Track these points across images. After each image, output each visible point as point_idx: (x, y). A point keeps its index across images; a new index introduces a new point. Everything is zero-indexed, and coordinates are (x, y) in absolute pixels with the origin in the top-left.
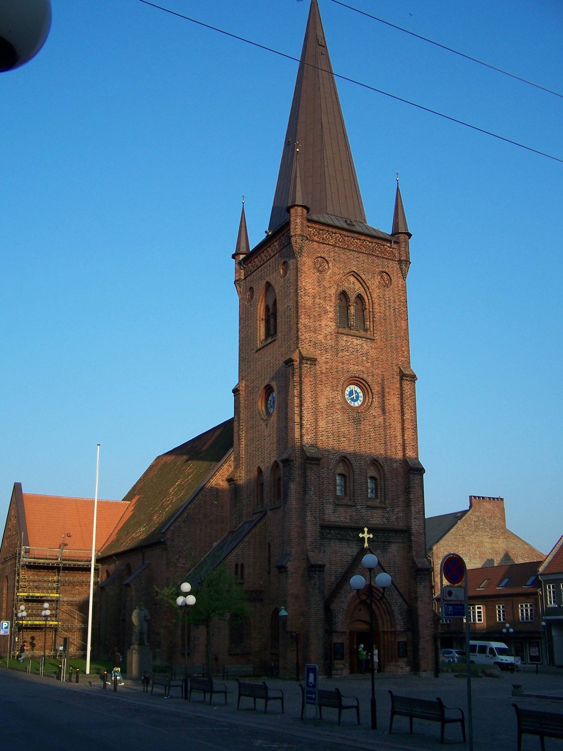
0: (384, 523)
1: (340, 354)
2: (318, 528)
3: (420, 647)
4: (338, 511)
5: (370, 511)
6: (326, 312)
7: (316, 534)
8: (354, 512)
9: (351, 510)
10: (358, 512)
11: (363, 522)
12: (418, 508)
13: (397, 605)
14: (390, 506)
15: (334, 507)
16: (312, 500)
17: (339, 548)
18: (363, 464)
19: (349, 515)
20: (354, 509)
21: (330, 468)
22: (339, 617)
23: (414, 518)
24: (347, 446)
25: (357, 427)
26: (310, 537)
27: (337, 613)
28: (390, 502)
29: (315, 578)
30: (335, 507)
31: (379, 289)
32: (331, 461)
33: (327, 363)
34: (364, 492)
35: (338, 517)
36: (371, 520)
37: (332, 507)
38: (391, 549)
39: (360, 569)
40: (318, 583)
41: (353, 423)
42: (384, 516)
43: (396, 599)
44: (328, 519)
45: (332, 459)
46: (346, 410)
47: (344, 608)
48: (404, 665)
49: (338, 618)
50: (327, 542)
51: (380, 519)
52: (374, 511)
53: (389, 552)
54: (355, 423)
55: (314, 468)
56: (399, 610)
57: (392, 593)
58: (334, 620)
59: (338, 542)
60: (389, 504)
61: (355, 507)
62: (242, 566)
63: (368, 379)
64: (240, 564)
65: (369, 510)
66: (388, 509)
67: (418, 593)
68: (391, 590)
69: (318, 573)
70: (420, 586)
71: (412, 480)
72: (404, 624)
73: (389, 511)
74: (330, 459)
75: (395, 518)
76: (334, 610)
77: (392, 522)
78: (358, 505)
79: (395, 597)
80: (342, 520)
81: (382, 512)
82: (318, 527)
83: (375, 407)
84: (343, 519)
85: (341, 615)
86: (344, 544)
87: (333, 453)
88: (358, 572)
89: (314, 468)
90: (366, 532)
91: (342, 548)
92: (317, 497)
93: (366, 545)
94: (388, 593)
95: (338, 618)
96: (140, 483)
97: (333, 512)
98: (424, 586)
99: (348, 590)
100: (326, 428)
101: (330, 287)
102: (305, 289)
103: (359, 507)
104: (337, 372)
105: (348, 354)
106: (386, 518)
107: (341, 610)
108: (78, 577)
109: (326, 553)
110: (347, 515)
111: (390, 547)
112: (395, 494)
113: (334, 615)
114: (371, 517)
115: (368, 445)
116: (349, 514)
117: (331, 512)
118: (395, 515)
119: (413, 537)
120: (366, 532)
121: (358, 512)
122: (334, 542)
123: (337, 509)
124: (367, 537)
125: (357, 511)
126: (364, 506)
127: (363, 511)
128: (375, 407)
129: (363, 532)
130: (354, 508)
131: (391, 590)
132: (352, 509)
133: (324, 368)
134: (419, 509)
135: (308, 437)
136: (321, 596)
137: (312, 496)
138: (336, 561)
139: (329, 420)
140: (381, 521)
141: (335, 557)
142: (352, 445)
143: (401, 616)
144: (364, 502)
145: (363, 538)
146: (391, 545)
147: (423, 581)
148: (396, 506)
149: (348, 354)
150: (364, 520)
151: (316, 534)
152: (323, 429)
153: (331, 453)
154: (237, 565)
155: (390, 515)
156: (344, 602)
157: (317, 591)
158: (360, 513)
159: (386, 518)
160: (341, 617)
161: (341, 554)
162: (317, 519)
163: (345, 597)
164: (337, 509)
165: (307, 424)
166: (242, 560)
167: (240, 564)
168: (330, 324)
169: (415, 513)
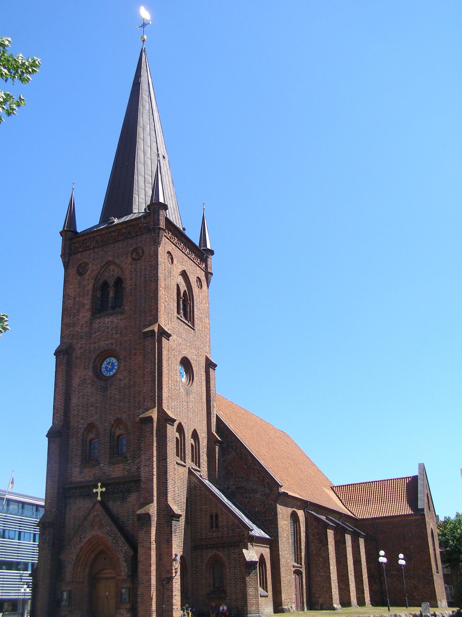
0: (125, 475)
1: (93, 336)
2: (56, 491)
3: (139, 593)
4: (84, 472)
5: (111, 467)
6: (84, 305)
7: (54, 496)
8: (98, 470)
9: (94, 469)
10: (101, 470)
11: (105, 477)
12: (148, 455)
13: (121, 552)
14: (131, 458)
15: (80, 469)
16: (53, 467)
17: (83, 504)
18: (108, 425)
19: (93, 474)
20: (97, 467)
21: (79, 436)
22: (68, 567)
23: (144, 466)
24: (94, 413)
25: (104, 394)
26: (49, 499)
27: (66, 563)
28: (131, 455)
29: (46, 534)
30: (81, 469)
31: (131, 265)
32: (80, 429)
33: (81, 348)
34: (107, 450)
35: (83, 478)
36: (112, 475)
37: (78, 470)
38: (131, 498)
39: (89, 521)
40: (48, 538)
41: (100, 391)
42: (125, 468)
43: (122, 546)
44: (75, 481)
45: (81, 428)
46: (95, 382)
47: (73, 559)
48: (126, 612)
49: (67, 567)
50: (73, 500)
51: (121, 472)
52: (115, 466)
53: (129, 502)
54: (102, 391)
55: (56, 440)
56: (124, 557)
57: (117, 541)
58: (64, 570)
59: (82, 499)
60: (130, 456)
61: (98, 466)
62: (217, 515)
63: (116, 348)
64: (214, 514)
65: (111, 466)
66: (129, 462)
67: (139, 539)
68: (117, 538)
69: (49, 530)
70: (141, 532)
71: (144, 429)
72: (128, 571)
73: (130, 463)
74: (79, 428)
75: (136, 469)
76: (65, 561)
77: (132, 473)
78: (102, 463)
79: (120, 545)
80: (87, 480)
81: (123, 466)
82: (56, 490)
83: (122, 371)
84: (87, 478)
85: (70, 565)
86: (87, 501)
87: (82, 423)
88: (87, 525)
89: (56, 440)
90: (99, 487)
91: (85, 504)
92: (56, 464)
93: (99, 498)
94: (113, 541)
95: (67, 567)
96: (251, 457)
97: (79, 474)
98: (145, 532)
99: (77, 542)
100: (77, 403)
101: (88, 284)
102: (68, 295)
103: (102, 465)
104: (90, 352)
105: (99, 333)
106: (126, 470)
107: (71, 561)
108: (32, 540)
109: (71, 511)
110: (91, 474)
111: (130, 496)
112: (136, 446)
113: (64, 565)
114: (112, 472)
115: (113, 407)
116: (93, 472)
117: (77, 474)
118: (136, 466)
119: (142, 485)
120: (99, 487)
121: (101, 470)
122: (78, 500)
123: (83, 471)
124: (100, 491)
125: (100, 468)
126: (107, 463)
127: (106, 467)
128: (122, 371)
129: (97, 487)
130: (98, 466)
131: (117, 538)
132: (96, 468)
133: (79, 353)
134: (149, 456)
135: (58, 415)
136: (49, 549)
137: (53, 464)
138: (80, 516)
139: (81, 395)
140: (122, 474)
141: (79, 513)
142: (99, 411)
143: (126, 563)
144: (107, 460)
145: (97, 493)
146: (131, 495)
147: (145, 527)
148: (137, 457)
149: (99, 333)
150: (106, 476)
151: (54, 496)
152: (75, 405)
153: (80, 423)
154: (211, 516)
155: (131, 466)
156: (73, 553)
157: (47, 545)
158: (103, 470)
159: (126, 470)
160: (69, 567)
161: (84, 509)
162: (56, 483)
163: (74, 548)
164: (83, 471)
165: (57, 405)
166: (216, 511)
167: (214, 514)
168: (86, 314)
169: (145, 460)
